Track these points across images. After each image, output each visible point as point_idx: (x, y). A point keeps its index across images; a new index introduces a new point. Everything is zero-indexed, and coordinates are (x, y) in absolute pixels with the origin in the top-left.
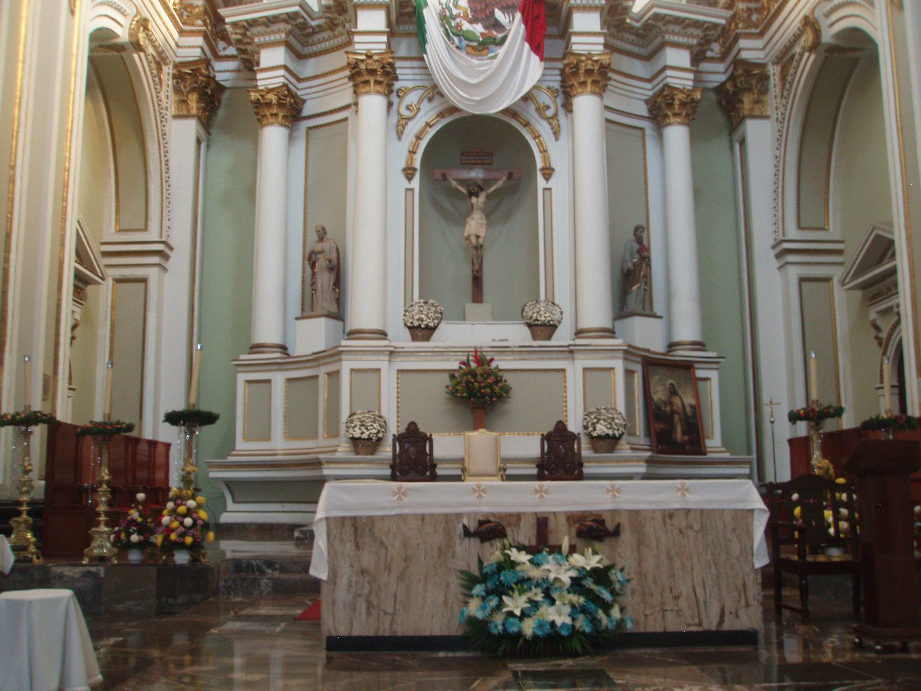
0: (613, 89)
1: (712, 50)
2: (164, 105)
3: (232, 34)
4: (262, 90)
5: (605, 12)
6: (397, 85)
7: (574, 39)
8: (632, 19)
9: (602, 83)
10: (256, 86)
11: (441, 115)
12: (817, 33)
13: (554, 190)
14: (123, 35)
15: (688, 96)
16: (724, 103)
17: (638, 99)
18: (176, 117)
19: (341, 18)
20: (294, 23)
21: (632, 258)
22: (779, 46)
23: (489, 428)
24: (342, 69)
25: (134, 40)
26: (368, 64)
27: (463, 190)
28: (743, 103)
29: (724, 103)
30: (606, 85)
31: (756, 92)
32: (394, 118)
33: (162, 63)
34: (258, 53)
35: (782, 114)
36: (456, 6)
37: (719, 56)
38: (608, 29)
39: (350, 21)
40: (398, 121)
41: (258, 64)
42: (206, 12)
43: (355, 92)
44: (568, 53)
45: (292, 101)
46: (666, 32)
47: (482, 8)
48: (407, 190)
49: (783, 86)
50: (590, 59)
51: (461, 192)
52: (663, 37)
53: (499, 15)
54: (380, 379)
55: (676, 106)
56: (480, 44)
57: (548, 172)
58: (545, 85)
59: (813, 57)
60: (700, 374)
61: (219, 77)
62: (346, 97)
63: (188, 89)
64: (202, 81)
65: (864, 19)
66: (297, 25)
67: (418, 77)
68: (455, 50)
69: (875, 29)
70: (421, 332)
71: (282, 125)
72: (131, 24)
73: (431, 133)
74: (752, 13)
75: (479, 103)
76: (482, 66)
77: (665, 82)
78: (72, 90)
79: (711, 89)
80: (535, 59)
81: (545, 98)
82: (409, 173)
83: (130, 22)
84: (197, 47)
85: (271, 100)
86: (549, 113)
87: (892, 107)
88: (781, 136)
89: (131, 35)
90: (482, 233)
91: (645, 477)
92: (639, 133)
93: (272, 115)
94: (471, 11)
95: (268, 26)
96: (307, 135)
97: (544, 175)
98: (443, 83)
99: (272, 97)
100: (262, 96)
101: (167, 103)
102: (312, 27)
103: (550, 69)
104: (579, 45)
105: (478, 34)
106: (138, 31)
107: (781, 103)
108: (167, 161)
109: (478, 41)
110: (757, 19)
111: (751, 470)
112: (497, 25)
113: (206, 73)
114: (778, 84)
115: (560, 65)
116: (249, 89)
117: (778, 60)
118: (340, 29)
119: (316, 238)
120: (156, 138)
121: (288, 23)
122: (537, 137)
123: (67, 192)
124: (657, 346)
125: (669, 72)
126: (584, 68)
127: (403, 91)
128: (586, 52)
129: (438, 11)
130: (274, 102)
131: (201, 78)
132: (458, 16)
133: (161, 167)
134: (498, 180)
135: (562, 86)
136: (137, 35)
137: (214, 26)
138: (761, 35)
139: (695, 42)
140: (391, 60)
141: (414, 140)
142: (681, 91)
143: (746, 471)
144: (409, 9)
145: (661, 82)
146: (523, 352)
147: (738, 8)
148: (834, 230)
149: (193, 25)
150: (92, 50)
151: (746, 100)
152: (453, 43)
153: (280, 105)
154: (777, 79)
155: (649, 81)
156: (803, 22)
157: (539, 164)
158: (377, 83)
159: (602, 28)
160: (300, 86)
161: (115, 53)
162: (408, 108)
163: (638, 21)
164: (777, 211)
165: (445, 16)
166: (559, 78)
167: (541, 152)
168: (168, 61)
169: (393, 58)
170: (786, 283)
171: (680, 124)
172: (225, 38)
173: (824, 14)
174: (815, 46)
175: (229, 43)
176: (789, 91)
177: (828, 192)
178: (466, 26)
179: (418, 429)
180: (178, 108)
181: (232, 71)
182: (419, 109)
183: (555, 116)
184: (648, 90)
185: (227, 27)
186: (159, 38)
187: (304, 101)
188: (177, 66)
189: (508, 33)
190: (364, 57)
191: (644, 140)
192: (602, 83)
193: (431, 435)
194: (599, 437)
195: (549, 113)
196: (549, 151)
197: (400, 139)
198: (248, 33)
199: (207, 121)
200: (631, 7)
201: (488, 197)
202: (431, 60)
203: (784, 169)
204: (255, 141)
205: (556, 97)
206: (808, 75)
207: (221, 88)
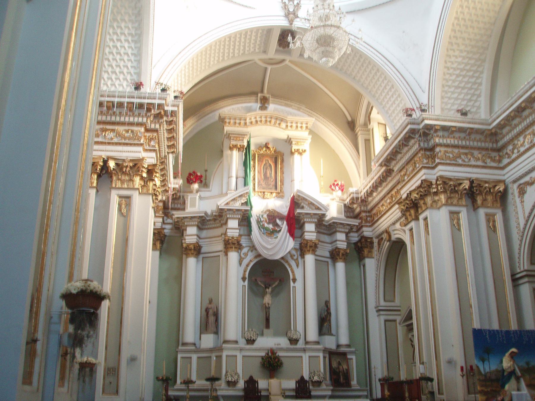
12: (390, 236)
16: (357, 249)
21: (324, 313)
23: (277, 378)
28: (364, 252)
51: (262, 287)
54: (237, 359)
57: (294, 280)
59: (388, 243)
60: (349, 357)
67: (247, 242)
68: (262, 235)
70: (250, 341)
73: (252, 264)
75: (271, 255)
79: (352, 243)
80: (291, 239)
82: (244, 279)
85: (191, 248)
90: (270, 303)
91: (331, 397)
92: (326, 263)
97: (293, 281)
105: (270, 229)
109: (271, 231)
110: (370, 220)
111: (368, 393)
112: (277, 225)
114: (377, 246)
117: (377, 237)
119: (208, 302)
122: (290, 266)
124: (333, 347)
125: (338, 242)
138: (370, 226)
143: (365, 393)
146: (288, 350)
148: (397, 302)
151: (365, 251)
164: (377, 294)
170: (380, 321)
177: (395, 288)
178: (266, 225)
179: (253, 379)
183: (297, 259)
184: (330, 247)
191: (328, 266)
193: (258, 381)
194: (315, 382)
195: (295, 258)
201: (272, 288)
203: (379, 279)
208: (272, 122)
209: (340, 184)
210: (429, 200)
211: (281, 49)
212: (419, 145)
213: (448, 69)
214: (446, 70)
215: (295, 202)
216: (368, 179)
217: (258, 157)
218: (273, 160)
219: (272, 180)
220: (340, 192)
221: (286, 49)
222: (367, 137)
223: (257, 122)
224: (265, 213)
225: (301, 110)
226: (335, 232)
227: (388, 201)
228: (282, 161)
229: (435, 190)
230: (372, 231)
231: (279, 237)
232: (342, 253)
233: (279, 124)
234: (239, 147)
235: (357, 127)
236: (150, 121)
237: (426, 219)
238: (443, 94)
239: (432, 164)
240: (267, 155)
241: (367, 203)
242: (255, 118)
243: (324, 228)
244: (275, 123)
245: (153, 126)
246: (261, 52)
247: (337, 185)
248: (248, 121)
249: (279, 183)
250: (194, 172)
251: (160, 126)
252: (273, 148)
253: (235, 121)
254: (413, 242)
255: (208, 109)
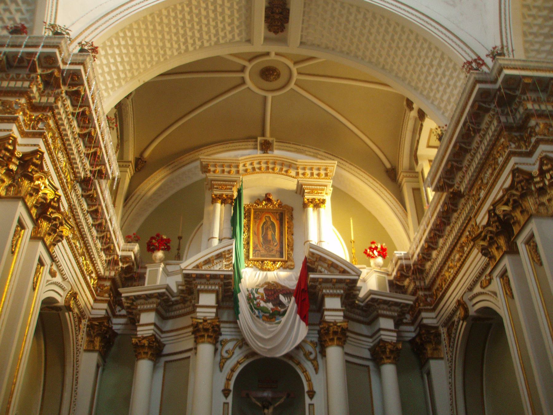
0: (349, 342)
1: (406, 318)
2: (80, 343)
3: (125, 303)
4: (140, 338)
5: (344, 297)
6: (221, 338)
7: (326, 313)
8: (358, 301)
9: (343, 339)
10: (136, 335)
11: (247, 357)
12: (466, 310)
13: (315, 406)
14: (61, 301)
15: (394, 346)
16: (415, 350)
17: (365, 348)
18: (85, 351)
19: (190, 297)
20: (162, 299)
22: (445, 317)
24: (188, 327)
25: (67, 304)
26: (204, 325)
27: (259, 404)
28: (427, 350)
29: (415, 350)
30: (345, 341)
31: (434, 343)
32: (218, 358)
33: (82, 318)
34: (139, 315)
35: (451, 357)
36: (257, 292)
37: (411, 322)
38: (345, 307)
39: (195, 299)
40: (221, 360)
41: (139, 321)
42: (111, 289)
43: (195, 341)
44: (322, 321)
45: (157, 345)
46: (379, 308)
47: (272, 294)
48: (224, 403)
49: (450, 339)
50: (336, 325)
52: (378, 312)
53: (282, 298)
55: (388, 353)
56: (271, 314)
57: (312, 394)
58: (309, 340)
59: (465, 323)
61: (115, 327)
62: (189, 343)
63: (95, 334)
64: (104, 330)
65: (490, 301)
66: (164, 300)
67: (233, 333)
68: (256, 318)
69: (500, 308)
71: (150, 359)
72: (67, 295)
73: (240, 368)
74: (427, 297)
75: (270, 350)
76: (273, 328)
77: (380, 338)
78: (26, 334)
80: (303, 324)
81: (309, 348)
82: (226, 392)
83: (66, 294)
84: (103, 309)
85: (145, 344)
86: (312, 357)
87: (516, 352)
88: (451, 370)
89: (66, 302)
93: (144, 353)
94: (266, 296)
95: (146, 300)
96: (165, 366)
98: (252, 343)
99: (146, 342)
100: (140, 341)
101: (81, 342)
102: (172, 301)
103: (312, 330)
104: (329, 317)
105: (270, 309)
106: (70, 300)
107: (449, 350)
108: (77, 378)
109: (270, 313)
112: (281, 304)
113: (108, 325)
115: (318, 328)
116: (132, 336)
117: (445, 325)
118: (188, 303)
120: (72, 363)
121: (158, 298)
122: (305, 371)
123: (12, 398)
126: (332, 330)
127: (224, 342)
128: (333, 321)
129: (246, 295)
130: (146, 344)
131: (104, 328)
132: (258, 298)
133: (73, 382)
134: (281, 398)
135: (319, 341)
136: (69, 302)
137: (115, 297)
138: (433, 310)
139: (396, 314)
140: (218, 323)
141: (230, 372)
142: (390, 343)
144: (229, 293)
145: (378, 338)
147: (419, 294)
149: (103, 296)
150: (41, 309)
152: (255, 314)
153: (150, 347)
154: (445, 336)
155: (371, 337)
156: (457, 304)
157: (306, 389)
158: (209, 337)
159: (342, 307)
160: (163, 335)
161: (54, 312)
162: (227, 352)
163: (362, 302)
165: (250, 298)
166: (318, 336)
167: (307, 381)
168: (85, 317)
169: (219, 321)
171: (390, 363)
172: (121, 304)
173: (469, 299)
174: (466, 317)
175: (123, 308)
176: (454, 343)
177: (483, 405)
178: (262, 304)
180: (88, 345)
181: (122, 324)
182: (233, 353)
183: (316, 358)
184: (370, 342)
185: (123, 299)
186: (82, 303)
187: (164, 345)
188: (90, 320)
189: (287, 309)
190: (201, 321)
192: (343, 339)
195: (312, 357)
196: (312, 381)
197: (221, 371)
198: (135, 303)
199: (104, 355)
200: (358, 294)
201: (275, 409)
202: (241, 323)
203: (455, 391)
204: (132, 368)
205: (316, 347)
206: (463, 335)
207: (115, 334)
208: (276, 169)
209: (379, 246)
210: (530, 203)
211: (272, 35)
212: (499, 122)
213: (529, 9)
214: (525, 11)
215: (308, 267)
216: (421, 232)
217: (255, 212)
218: (278, 217)
219: (275, 244)
220: (380, 260)
221: (280, 35)
222: (415, 185)
223: (254, 169)
224: (262, 287)
225: (319, 156)
226: (379, 316)
227: (457, 256)
228: (291, 218)
229: (541, 185)
230: (436, 317)
231: (282, 322)
232: (390, 349)
233: (287, 171)
234: (226, 198)
235: (399, 173)
236: (39, 89)
237: (530, 241)
238: (527, 45)
239: (526, 148)
240: (268, 211)
241: (425, 274)
242: (252, 164)
243: (358, 311)
244: (281, 170)
245: (44, 100)
246: (244, 40)
247: (376, 248)
248: (241, 168)
249: (286, 247)
250: (158, 235)
251: (56, 99)
252: (278, 200)
253: (223, 169)
254: (512, 293)
255: (187, 158)
